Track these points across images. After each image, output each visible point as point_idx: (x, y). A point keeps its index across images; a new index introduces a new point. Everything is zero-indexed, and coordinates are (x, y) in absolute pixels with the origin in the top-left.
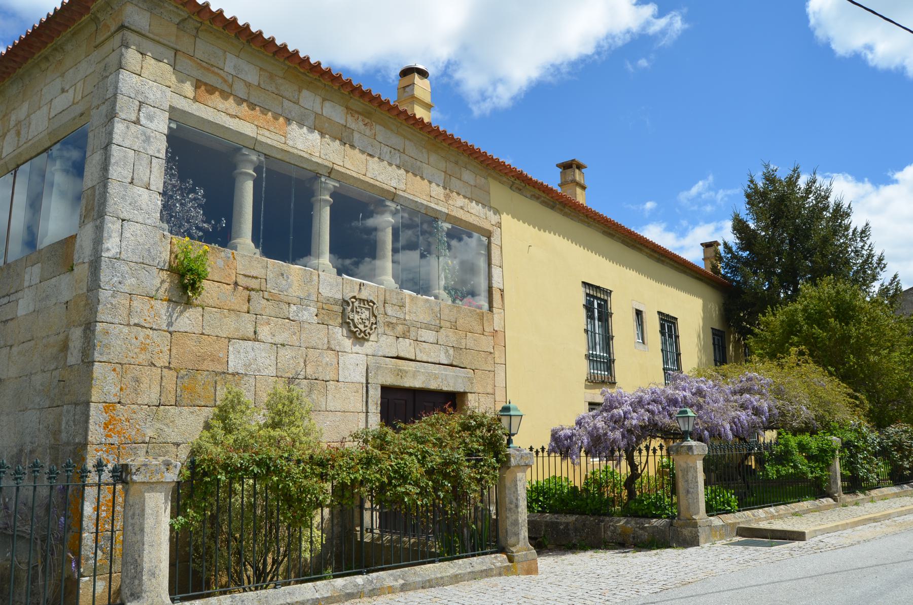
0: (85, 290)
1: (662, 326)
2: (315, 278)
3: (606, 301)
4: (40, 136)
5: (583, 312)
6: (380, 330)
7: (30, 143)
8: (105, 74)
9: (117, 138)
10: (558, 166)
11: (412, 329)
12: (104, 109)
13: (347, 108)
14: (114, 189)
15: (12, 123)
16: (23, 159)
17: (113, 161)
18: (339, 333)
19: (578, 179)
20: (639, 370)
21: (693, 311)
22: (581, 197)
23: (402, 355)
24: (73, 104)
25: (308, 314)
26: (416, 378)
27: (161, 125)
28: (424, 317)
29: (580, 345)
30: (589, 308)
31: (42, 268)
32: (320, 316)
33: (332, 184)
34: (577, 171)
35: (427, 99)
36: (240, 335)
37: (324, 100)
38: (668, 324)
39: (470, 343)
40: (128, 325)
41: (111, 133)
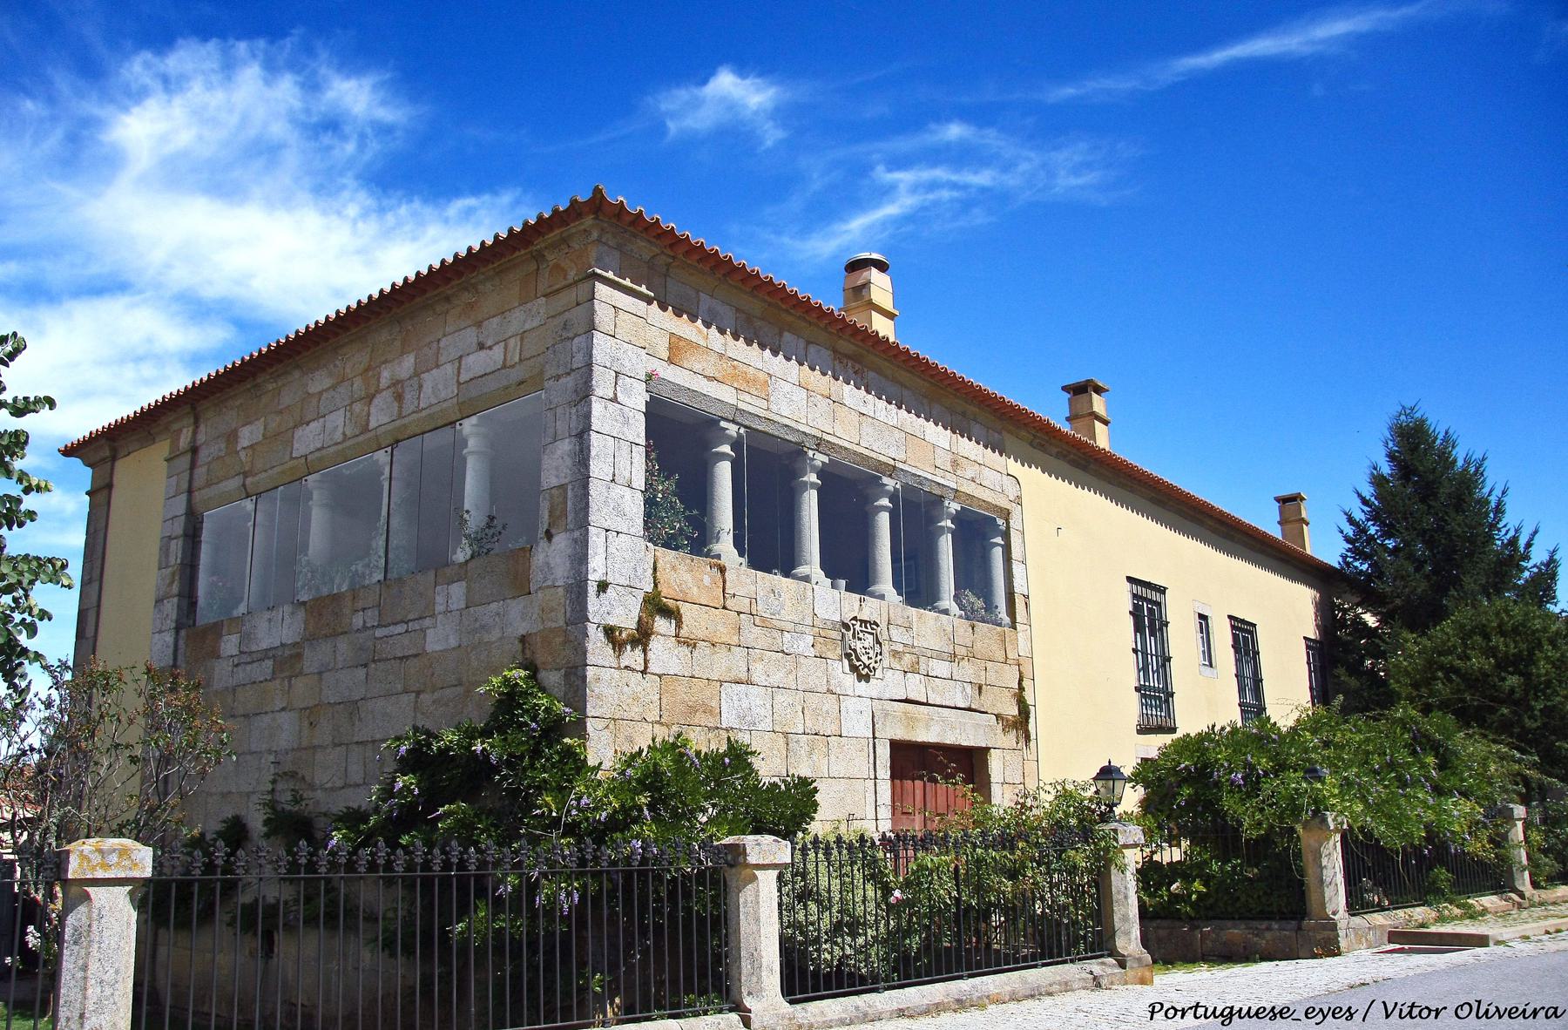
0: (561, 623)
1: (1235, 637)
2: (809, 593)
3: (1159, 604)
4: (445, 405)
5: (1130, 621)
6: (886, 663)
7: (424, 413)
8: (565, 335)
9: (596, 423)
10: (1064, 388)
11: (922, 659)
12: (569, 382)
13: (835, 351)
14: (595, 489)
15: (384, 382)
16: (409, 432)
17: (593, 453)
18: (840, 669)
19: (1096, 409)
20: (1206, 703)
21: (1287, 615)
22: (1103, 438)
23: (911, 697)
24: (504, 367)
25: (804, 645)
26: (930, 731)
27: (637, 399)
28: (936, 643)
29: (1129, 675)
30: (1136, 613)
31: (469, 589)
32: (818, 646)
33: (820, 459)
34: (1095, 396)
35: (888, 305)
36: (732, 676)
37: (808, 343)
38: (1244, 636)
39: (992, 678)
40: (619, 668)
41: (588, 416)
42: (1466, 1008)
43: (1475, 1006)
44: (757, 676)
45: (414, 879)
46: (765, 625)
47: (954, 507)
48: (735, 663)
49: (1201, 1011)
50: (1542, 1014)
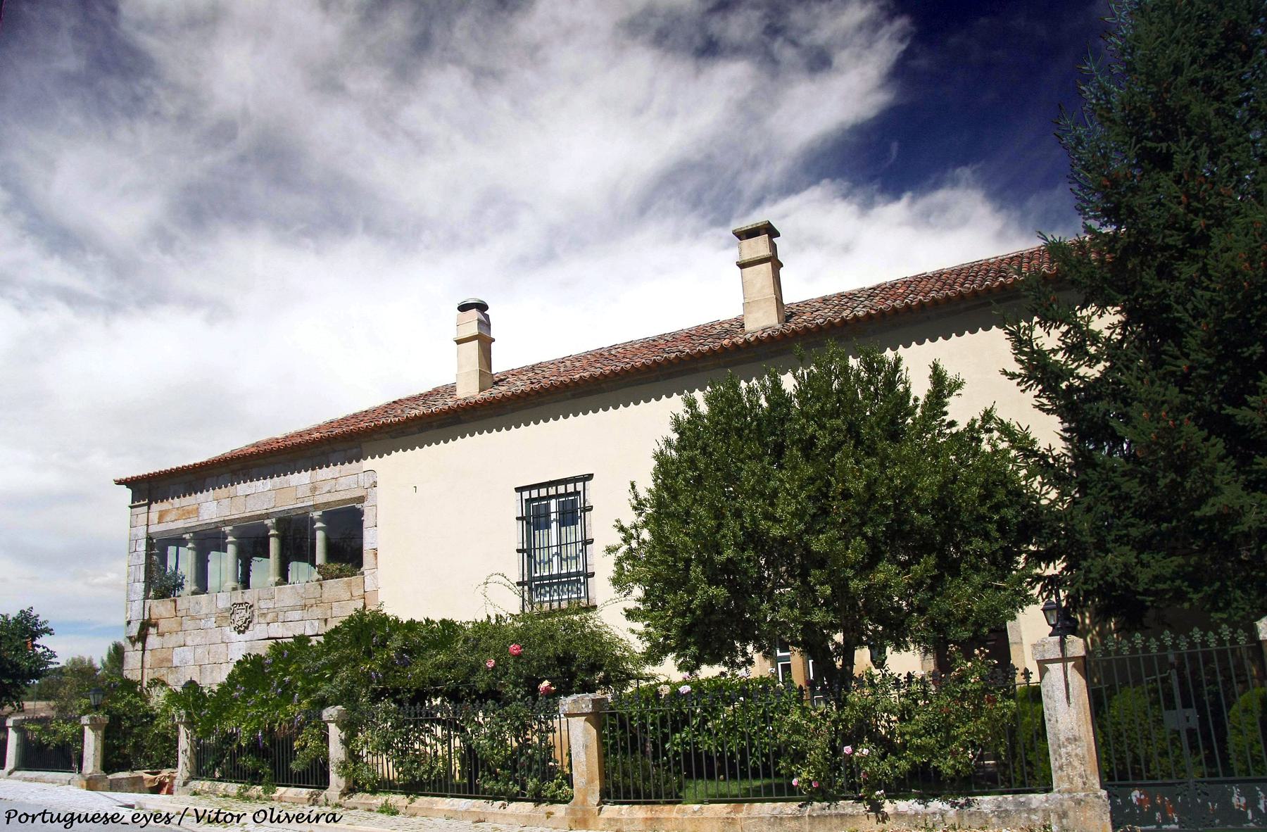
25: (211, 623)
42: (262, 815)
43: (269, 812)
44: (189, 642)
45: (1226, 651)
46: (193, 618)
47: (316, 515)
48: (180, 638)
49: (47, 817)
50: (322, 820)
